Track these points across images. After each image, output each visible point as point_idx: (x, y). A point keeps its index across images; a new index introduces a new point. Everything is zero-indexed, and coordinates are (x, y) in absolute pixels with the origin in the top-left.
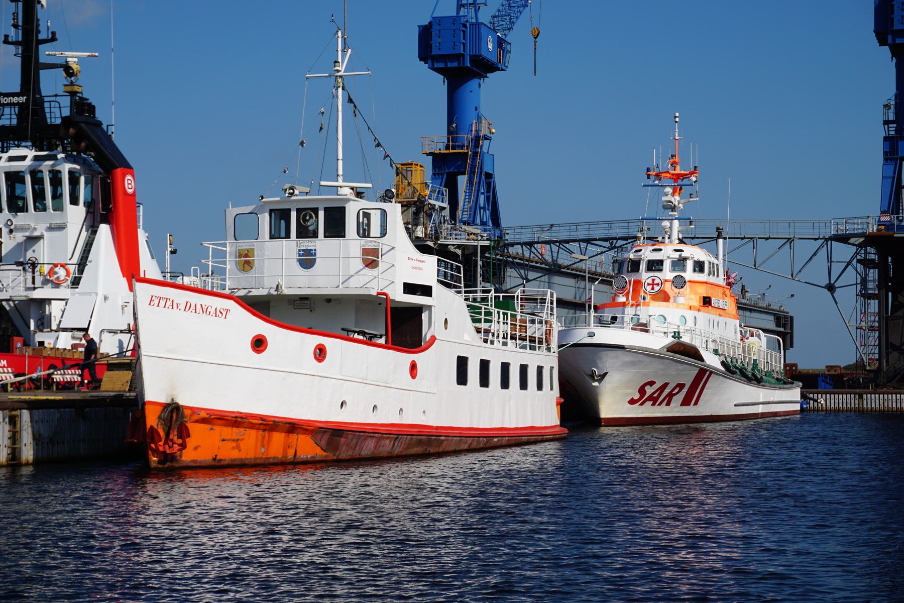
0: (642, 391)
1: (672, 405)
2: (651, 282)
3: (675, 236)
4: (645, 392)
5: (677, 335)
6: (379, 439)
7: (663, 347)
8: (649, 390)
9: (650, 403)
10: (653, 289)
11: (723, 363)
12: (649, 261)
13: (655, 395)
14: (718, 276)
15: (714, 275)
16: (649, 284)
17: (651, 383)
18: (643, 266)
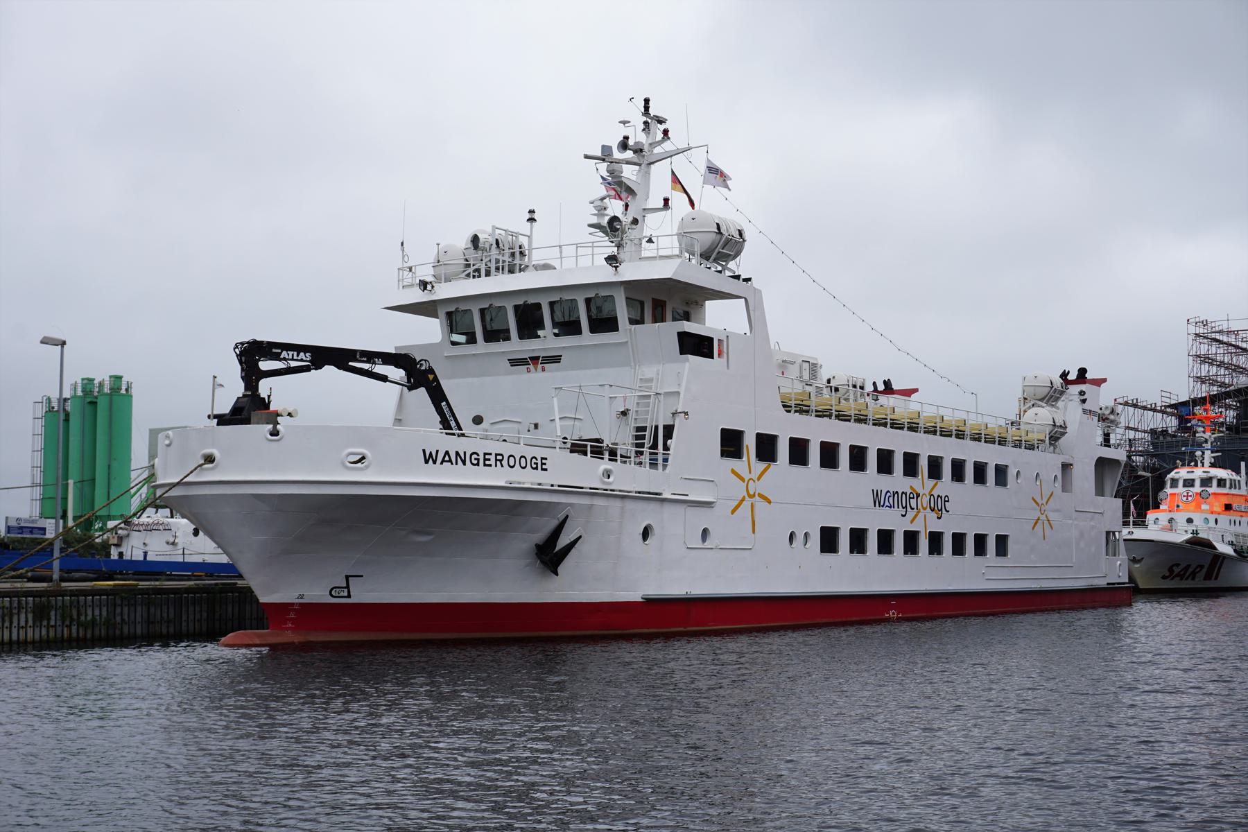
0: (1171, 570)
1: (1197, 579)
2: (1186, 494)
3: (1207, 463)
4: (1173, 571)
5: (1195, 532)
6: (48, 597)
7: (1184, 541)
8: (1176, 570)
9: (1179, 578)
10: (1187, 499)
11: (1235, 551)
12: (1185, 480)
13: (1182, 573)
14: (1240, 488)
15: (1235, 488)
16: (1184, 496)
17: (1178, 565)
18: (1181, 483)
